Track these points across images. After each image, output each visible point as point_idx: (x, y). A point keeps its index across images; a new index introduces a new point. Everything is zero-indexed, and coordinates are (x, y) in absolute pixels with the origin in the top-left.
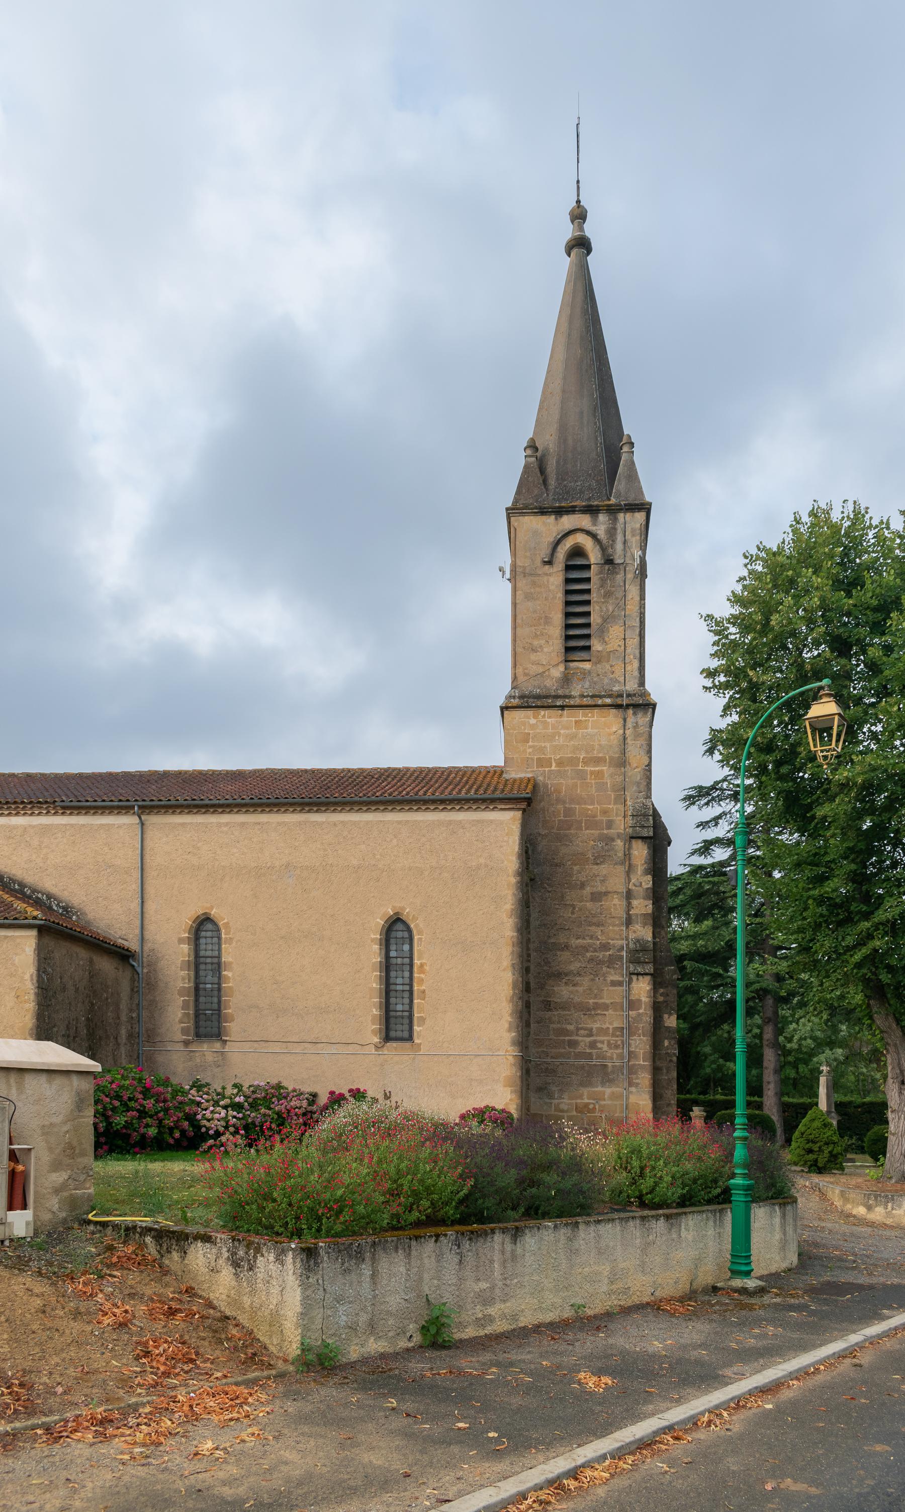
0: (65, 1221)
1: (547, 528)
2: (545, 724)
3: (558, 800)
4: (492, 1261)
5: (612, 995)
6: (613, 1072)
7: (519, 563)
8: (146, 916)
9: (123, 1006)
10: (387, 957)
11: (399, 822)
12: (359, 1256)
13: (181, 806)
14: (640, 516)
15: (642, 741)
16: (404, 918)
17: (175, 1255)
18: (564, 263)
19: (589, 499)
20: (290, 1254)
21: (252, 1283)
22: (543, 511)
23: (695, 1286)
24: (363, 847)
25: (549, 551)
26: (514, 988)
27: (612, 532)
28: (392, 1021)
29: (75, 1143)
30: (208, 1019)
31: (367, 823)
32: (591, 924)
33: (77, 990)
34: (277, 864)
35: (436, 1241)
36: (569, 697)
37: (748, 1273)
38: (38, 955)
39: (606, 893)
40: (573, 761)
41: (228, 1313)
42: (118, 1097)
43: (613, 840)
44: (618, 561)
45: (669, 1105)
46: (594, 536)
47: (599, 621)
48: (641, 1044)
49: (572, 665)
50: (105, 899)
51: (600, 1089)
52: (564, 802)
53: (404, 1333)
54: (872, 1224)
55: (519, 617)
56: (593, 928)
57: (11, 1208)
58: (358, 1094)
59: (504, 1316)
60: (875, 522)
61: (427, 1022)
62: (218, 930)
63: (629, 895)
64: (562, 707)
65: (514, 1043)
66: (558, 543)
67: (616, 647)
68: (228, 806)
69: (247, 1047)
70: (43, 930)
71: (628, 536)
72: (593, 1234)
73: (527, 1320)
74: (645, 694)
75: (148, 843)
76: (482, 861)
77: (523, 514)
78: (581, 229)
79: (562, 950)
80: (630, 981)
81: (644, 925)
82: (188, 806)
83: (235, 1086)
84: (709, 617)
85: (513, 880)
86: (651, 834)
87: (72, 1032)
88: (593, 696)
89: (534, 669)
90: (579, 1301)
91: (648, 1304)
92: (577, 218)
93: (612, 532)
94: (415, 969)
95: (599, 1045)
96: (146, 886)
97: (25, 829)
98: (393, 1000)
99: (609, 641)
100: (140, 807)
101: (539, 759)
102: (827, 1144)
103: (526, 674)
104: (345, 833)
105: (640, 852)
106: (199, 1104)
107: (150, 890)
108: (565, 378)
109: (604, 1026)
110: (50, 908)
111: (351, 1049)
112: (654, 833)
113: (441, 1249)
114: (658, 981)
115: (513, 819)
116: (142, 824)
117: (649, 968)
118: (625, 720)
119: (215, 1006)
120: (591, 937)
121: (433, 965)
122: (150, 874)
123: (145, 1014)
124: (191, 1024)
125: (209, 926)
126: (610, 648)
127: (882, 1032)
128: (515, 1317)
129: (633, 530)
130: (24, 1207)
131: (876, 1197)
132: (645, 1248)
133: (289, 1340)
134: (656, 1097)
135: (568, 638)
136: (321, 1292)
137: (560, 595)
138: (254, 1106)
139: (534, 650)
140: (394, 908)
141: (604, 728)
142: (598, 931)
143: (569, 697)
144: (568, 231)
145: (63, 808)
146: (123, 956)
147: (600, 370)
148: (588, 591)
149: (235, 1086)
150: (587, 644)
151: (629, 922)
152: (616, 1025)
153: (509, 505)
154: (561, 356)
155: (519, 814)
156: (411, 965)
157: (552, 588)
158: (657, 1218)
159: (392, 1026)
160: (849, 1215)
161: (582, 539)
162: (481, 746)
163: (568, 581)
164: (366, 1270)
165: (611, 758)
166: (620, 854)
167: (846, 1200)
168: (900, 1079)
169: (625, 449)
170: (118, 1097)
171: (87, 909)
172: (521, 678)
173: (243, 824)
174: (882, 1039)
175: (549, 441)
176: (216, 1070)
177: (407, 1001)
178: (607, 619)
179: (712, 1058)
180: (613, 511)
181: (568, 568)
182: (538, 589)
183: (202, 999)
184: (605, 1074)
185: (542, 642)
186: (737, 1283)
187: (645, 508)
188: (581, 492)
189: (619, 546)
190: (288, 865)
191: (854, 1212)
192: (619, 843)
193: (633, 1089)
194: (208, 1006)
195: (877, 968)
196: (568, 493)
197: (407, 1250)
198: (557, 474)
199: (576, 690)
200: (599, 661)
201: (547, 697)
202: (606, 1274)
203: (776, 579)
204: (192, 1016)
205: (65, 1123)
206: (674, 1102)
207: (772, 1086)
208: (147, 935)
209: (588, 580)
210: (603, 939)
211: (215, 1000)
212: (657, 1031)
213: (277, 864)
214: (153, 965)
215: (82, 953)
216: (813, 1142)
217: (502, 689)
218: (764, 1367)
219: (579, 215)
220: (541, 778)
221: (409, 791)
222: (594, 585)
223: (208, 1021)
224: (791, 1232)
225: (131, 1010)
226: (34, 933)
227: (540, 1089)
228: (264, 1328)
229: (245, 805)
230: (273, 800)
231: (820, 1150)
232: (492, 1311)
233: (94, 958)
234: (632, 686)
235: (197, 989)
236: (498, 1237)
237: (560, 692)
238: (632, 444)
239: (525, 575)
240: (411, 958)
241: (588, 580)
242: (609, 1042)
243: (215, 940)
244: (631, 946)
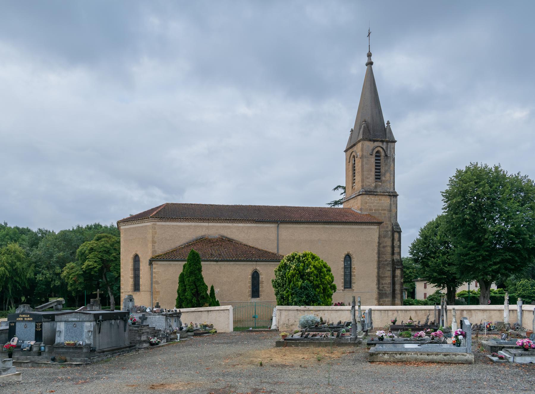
15: (395, 205)
22: (370, 140)
27: (387, 148)
39: (386, 246)
40: (378, 210)
66: (373, 149)
74: (396, 192)
75: (280, 233)
93: (387, 148)
97: (243, 227)
99: (386, 177)
107: (280, 246)
137: (374, 164)
139: (368, 179)
141: (386, 201)
142: (384, 256)
161: (379, 149)
172: (365, 186)
178: (386, 171)
181: (376, 156)
189: (389, 152)
210: (386, 258)
234: (392, 190)
237: (375, 190)
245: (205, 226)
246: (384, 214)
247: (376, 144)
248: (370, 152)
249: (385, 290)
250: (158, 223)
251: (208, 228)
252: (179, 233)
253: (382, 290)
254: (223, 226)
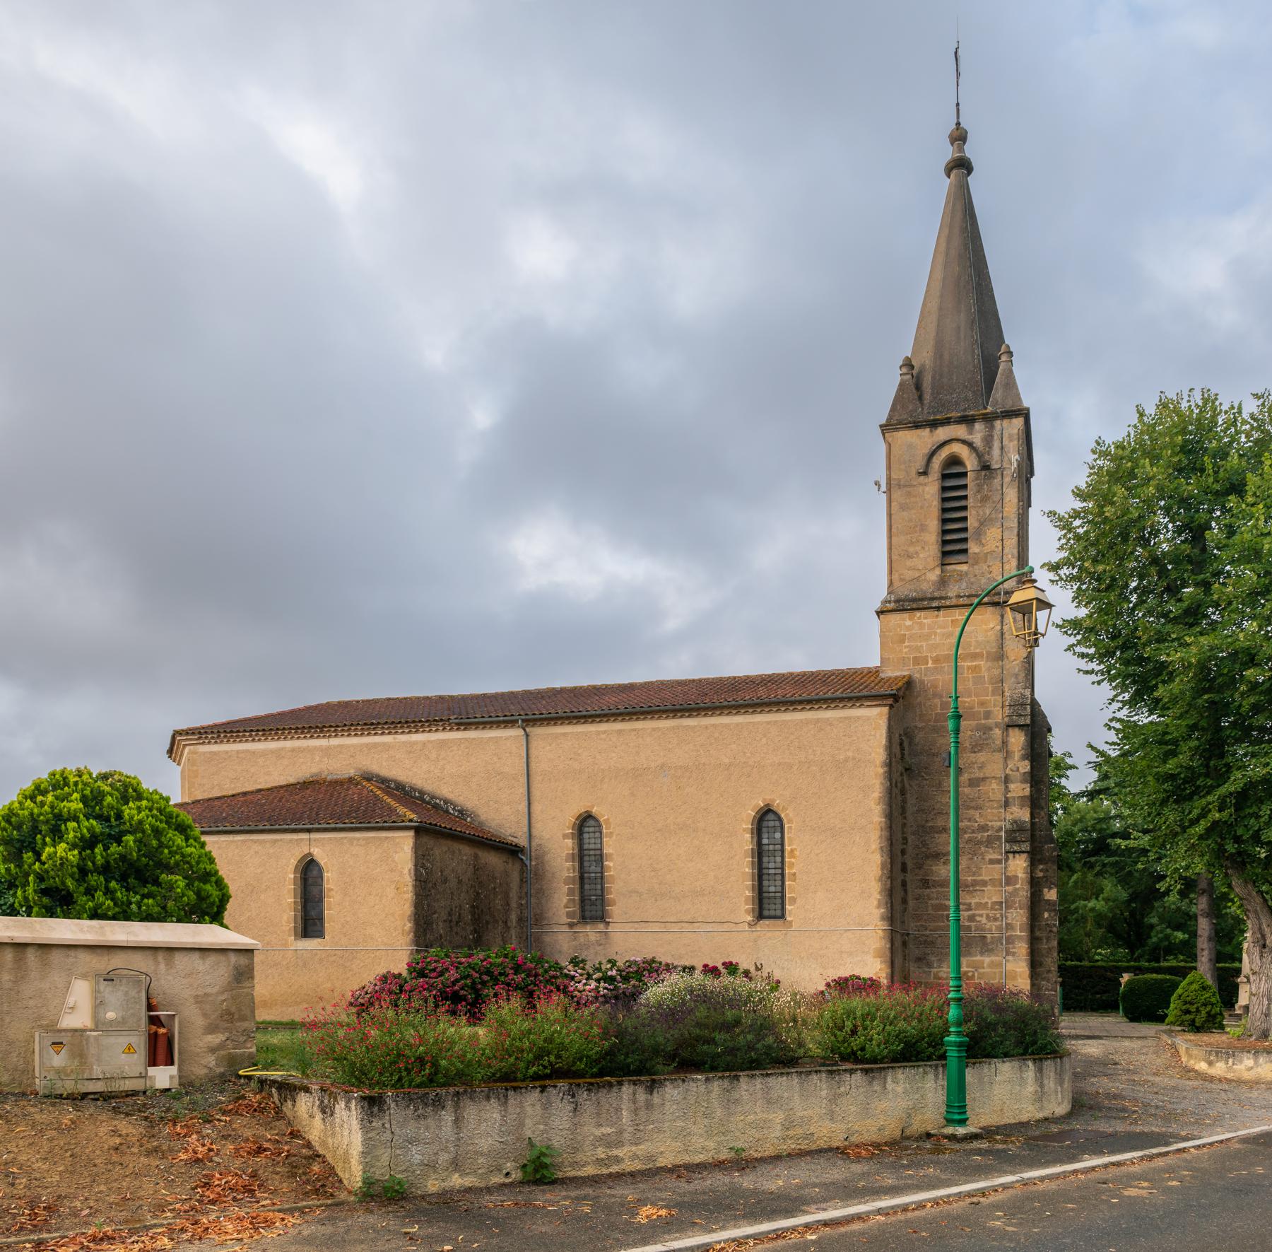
0: (222, 1075)
1: (923, 440)
2: (921, 625)
3: (935, 695)
4: (619, 1109)
5: (989, 872)
6: (992, 943)
7: (894, 476)
8: (533, 815)
9: (514, 894)
10: (760, 844)
11: (768, 723)
12: (438, 1104)
13: (561, 718)
14: (1018, 422)
16: (774, 809)
17: (289, 1103)
18: (945, 184)
19: (965, 410)
20: (354, 1102)
21: (333, 1125)
22: (917, 425)
23: (908, 1132)
24: (734, 746)
25: (924, 463)
26: (882, 869)
27: (988, 440)
28: (765, 901)
29: (233, 1009)
30: (593, 904)
31: (737, 725)
32: (969, 808)
33: (460, 882)
34: (653, 765)
35: (542, 1092)
36: (946, 598)
37: (962, 1122)
38: (416, 853)
39: (984, 779)
41: (321, 1152)
42: (488, 972)
43: (991, 729)
44: (995, 466)
45: (1049, 971)
46: (969, 444)
47: (976, 524)
48: (1018, 917)
49: (949, 568)
50: (496, 802)
51: (979, 958)
52: (941, 696)
53: (500, 1170)
54: (1211, 1079)
55: (894, 527)
56: (971, 812)
57: (153, 1062)
58: (731, 968)
59: (635, 1157)
60: (1225, 408)
61: (798, 901)
62: (600, 826)
63: (1007, 780)
64: (938, 608)
65: (883, 919)
66: (933, 454)
67: (993, 548)
68: (605, 715)
69: (628, 927)
70: (419, 831)
71: (1005, 442)
72: (759, 1086)
73: (666, 1161)
75: (533, 752)
76: (850, 754)
77: (897, 430)
78: (961, 149)
79: (940, 832)
80: (1007, 860)
81: (1022, 806)
82: (568, 718)
83: (610, 961)
84: (1052, 513)
85: (881, 771)
86: (1028, 722)
87: (455, 918)
88: (969, 596)
89: (909, 574)
90: (740, 1145)
91: (838, 1148)
92: (956, 140)
93: (988, 440)
94: (786, 854)
95: (978, 919)
96: (533, 790)
98: (766, 883)
100: (523, 721)
101: (915, 658)
102: (1205, 1005)
103: (901, 580)
104: (716, 735)
105: (1018, 739)
106: (573, 978)
107: (536, 794)
108: (942, 296)
109: (983, 901)
110: (447, 811)
111: (726, 927)
112: (1032, 720)
113: (548, 1098)
114: (1035, 858)
115: (880, 714)
116: (527, 736)
117: (1026, 846)
118: (1002, 616)
119: (599, 892)
120: (969, 820)
121: (801, 850)
122: (536, 780)
123: (533, 900)
124: (577, 909)
125: (592, 822)
126: (987, 549)
127: (1241, 899)
128: (651, 1158)
129: (1010, 436)
130: (170, 1062)
131: (1217, 1053)
132: (834, 1099)
133: (353, 1175)
134: (1035, 964)
135: (945, 543)
136: (388, 1135)
138: (626, 979)
139: (910, 557)
140: (764, 800)
142: (976, 814)
143: (946, 598)
144: (948, 153)
145: (457, 724)
146: (512, 851)
147: (979, 284)
148: (965, 497)
149: (610, 961)
150: (964, 547)
151: (1007, 804)
152: (994, 899)
153: (884, 422)
154: (939, 275)
155: (886, 710)
156: (783, 851)
157: (927, 497)
158: (851, 1072)
159: (766, 906)
160: (1193, 1070)
161: (957, 449)
162: (861, 647)
163: (944, 489)
164: (448, 1116)
165: (988, 653)
166: (999, 742)
167: (1190, 1056)
168: (1261, 942)
169: (1004, 358)
170: (488, 972)
171: (480, 812)
172: (897, 584)
173: (620, 732)
174: (1241, 906)
175: (925, 359)
176: (598, 948)
177: (779, 883)
179: (1158, 928)
180: (989, 419)
181: (945, 477)
182: (913, 499)
183: (587, 887)
184: (984, 945)
185: (918, 548)
186: (949, 1130)
187: (1025, 414)
188: (957, 403)
189: (996, 452)
190: (662, 766)
191: (1197, 1067)
192: (997, 732)
193: (1010, 958)
194: (593, 892)
195: (1223, 839)
196: (943, 405)
197: (503, 1099)
198: (933, 388)
199: (952, 591)
200: (977, 563)
201: (922, 600)
202: (778, 1121)
203: (1118, 470)
204: (577, 902)
205: (222, 993)
206: (1054, 968)
207: (1206, 953)
208: (534, 832)
209: (965, 486)
210: (981, 821)
211: (599, 887)
212: (1035, 905)
213: (653, 765)
214: (540, 858)
215: (467, 850)
216: (1191, 1004)
217: (880, 593)
218: (849, 1206)
219: (959, 137)
220: (917, 675)
221: (789, 692)
222: (970, 492)
223: (592, 905)
224: (1052, 1085)
225: (520, 898)
226: (411, 833)
227: (919, 959)
228: (341, 1165)
229: (621, 714)
230: (646, 709)
231: (1198, 1011)
232: (619, 1152)
233: (480, 853)
235: (582, 878)
236: (627, 1089)
237: (936, 594)
238: (1010, 354)
239: (899, 486)
240: (782, 845)
241: (965, 486)
242: (988, 916)
243: (597, 834)
244: (1009, 826)
245: (321, 749)
246: (976, 669)
247: (943, 433)
248: (919, 464)
249: (980, 928)
250: (202, 749)
251: (327, 751)
252: (253, 770)
253: (969, 928)
254: (367, 745)
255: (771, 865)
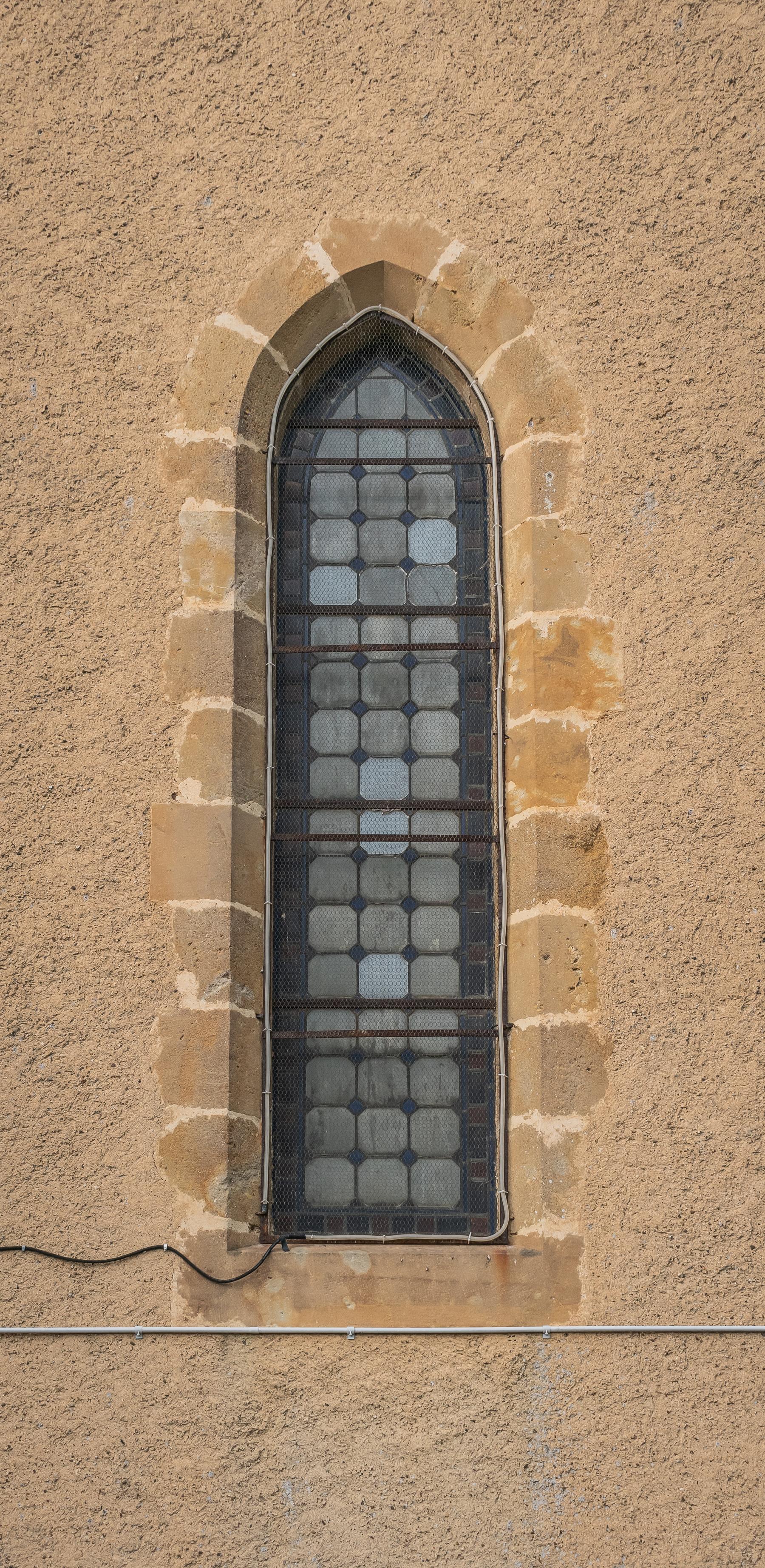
16: (422, 315)
28: (327, 1078)
61: (626, 1072)
94: (516, 676)
159: (329, 1122)
255: (382, 766)
